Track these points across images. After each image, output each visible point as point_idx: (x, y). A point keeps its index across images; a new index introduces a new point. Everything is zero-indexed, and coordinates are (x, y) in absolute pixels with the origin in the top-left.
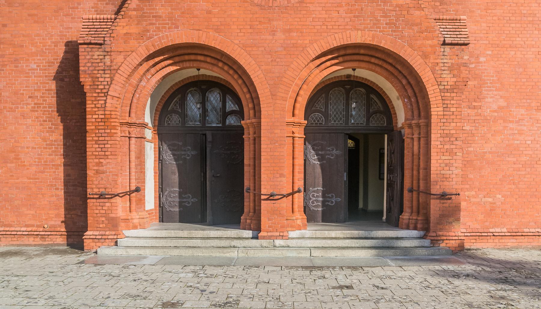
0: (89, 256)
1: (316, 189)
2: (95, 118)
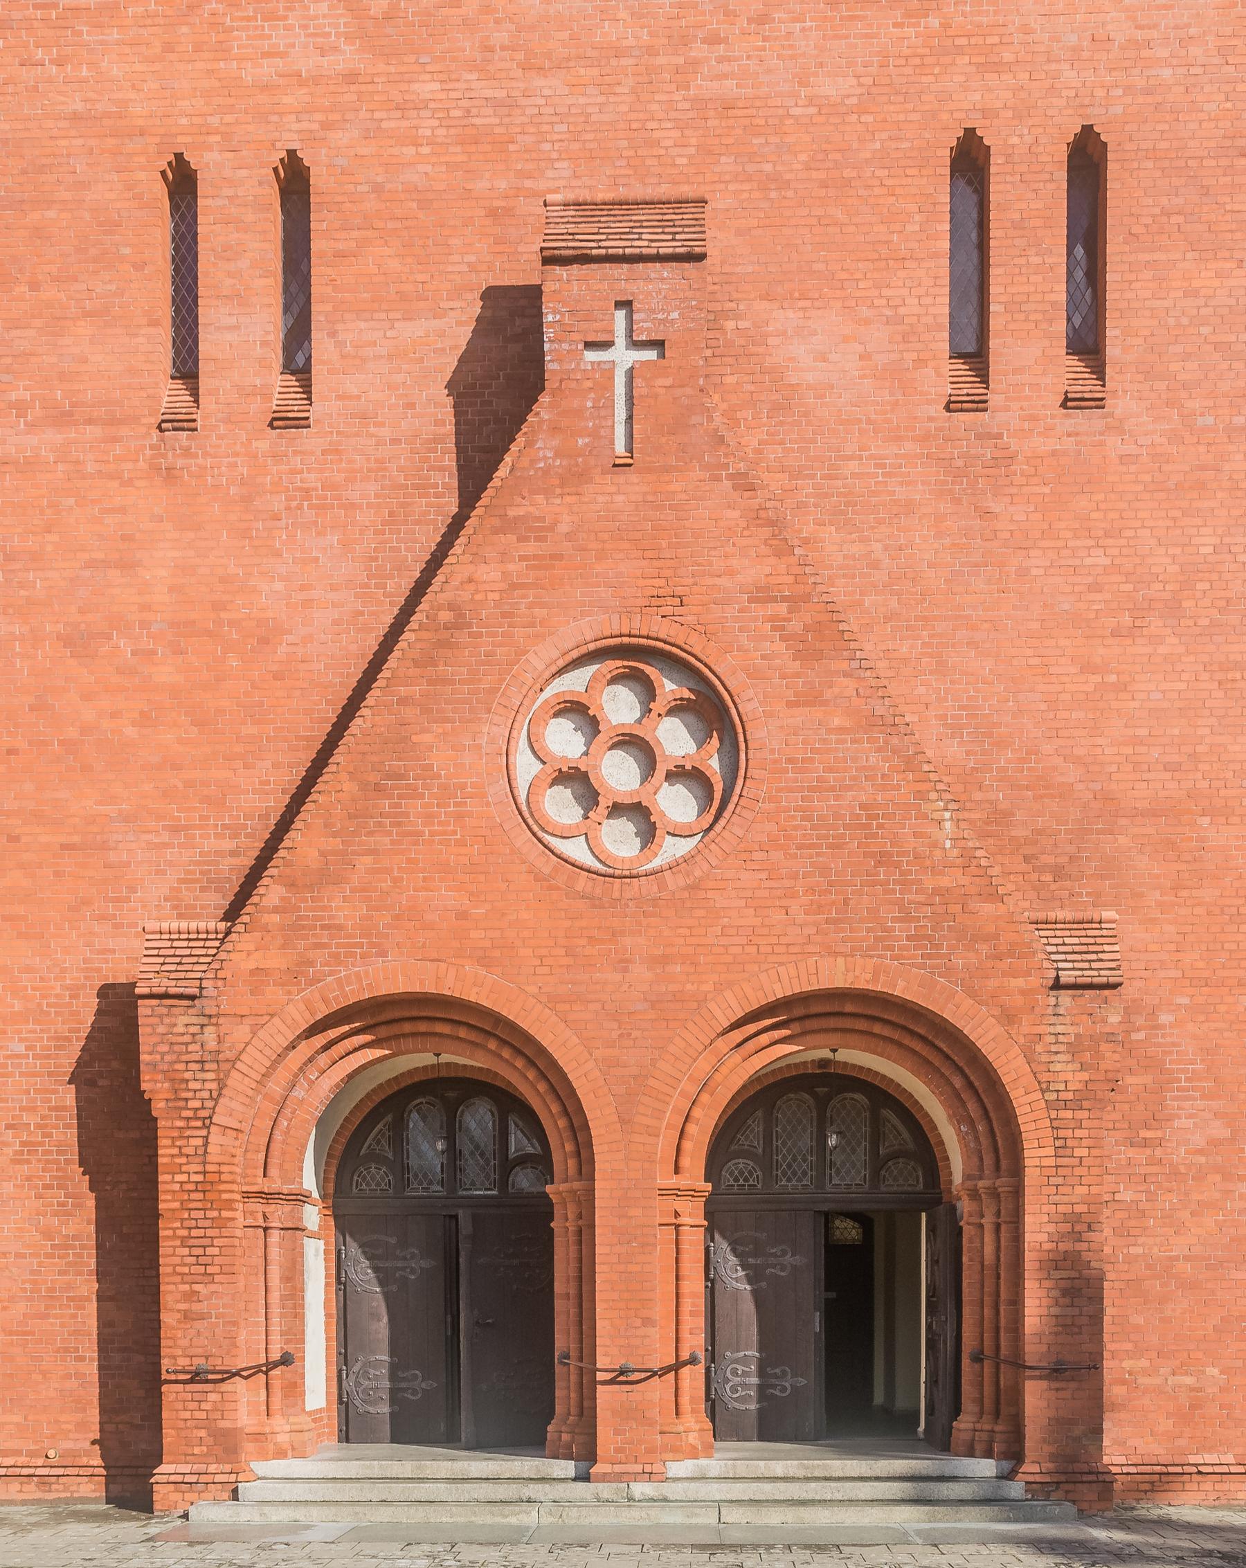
0: (170, 1525)
1: (742, 1354)
2: (181, 1183)
